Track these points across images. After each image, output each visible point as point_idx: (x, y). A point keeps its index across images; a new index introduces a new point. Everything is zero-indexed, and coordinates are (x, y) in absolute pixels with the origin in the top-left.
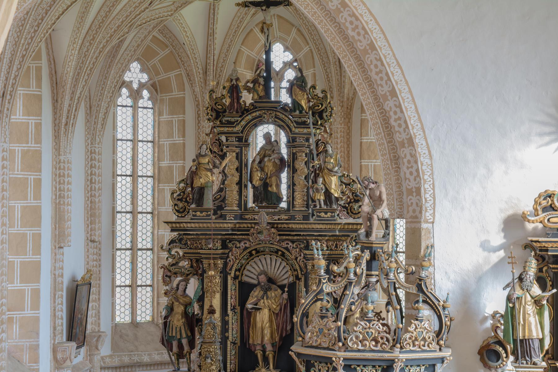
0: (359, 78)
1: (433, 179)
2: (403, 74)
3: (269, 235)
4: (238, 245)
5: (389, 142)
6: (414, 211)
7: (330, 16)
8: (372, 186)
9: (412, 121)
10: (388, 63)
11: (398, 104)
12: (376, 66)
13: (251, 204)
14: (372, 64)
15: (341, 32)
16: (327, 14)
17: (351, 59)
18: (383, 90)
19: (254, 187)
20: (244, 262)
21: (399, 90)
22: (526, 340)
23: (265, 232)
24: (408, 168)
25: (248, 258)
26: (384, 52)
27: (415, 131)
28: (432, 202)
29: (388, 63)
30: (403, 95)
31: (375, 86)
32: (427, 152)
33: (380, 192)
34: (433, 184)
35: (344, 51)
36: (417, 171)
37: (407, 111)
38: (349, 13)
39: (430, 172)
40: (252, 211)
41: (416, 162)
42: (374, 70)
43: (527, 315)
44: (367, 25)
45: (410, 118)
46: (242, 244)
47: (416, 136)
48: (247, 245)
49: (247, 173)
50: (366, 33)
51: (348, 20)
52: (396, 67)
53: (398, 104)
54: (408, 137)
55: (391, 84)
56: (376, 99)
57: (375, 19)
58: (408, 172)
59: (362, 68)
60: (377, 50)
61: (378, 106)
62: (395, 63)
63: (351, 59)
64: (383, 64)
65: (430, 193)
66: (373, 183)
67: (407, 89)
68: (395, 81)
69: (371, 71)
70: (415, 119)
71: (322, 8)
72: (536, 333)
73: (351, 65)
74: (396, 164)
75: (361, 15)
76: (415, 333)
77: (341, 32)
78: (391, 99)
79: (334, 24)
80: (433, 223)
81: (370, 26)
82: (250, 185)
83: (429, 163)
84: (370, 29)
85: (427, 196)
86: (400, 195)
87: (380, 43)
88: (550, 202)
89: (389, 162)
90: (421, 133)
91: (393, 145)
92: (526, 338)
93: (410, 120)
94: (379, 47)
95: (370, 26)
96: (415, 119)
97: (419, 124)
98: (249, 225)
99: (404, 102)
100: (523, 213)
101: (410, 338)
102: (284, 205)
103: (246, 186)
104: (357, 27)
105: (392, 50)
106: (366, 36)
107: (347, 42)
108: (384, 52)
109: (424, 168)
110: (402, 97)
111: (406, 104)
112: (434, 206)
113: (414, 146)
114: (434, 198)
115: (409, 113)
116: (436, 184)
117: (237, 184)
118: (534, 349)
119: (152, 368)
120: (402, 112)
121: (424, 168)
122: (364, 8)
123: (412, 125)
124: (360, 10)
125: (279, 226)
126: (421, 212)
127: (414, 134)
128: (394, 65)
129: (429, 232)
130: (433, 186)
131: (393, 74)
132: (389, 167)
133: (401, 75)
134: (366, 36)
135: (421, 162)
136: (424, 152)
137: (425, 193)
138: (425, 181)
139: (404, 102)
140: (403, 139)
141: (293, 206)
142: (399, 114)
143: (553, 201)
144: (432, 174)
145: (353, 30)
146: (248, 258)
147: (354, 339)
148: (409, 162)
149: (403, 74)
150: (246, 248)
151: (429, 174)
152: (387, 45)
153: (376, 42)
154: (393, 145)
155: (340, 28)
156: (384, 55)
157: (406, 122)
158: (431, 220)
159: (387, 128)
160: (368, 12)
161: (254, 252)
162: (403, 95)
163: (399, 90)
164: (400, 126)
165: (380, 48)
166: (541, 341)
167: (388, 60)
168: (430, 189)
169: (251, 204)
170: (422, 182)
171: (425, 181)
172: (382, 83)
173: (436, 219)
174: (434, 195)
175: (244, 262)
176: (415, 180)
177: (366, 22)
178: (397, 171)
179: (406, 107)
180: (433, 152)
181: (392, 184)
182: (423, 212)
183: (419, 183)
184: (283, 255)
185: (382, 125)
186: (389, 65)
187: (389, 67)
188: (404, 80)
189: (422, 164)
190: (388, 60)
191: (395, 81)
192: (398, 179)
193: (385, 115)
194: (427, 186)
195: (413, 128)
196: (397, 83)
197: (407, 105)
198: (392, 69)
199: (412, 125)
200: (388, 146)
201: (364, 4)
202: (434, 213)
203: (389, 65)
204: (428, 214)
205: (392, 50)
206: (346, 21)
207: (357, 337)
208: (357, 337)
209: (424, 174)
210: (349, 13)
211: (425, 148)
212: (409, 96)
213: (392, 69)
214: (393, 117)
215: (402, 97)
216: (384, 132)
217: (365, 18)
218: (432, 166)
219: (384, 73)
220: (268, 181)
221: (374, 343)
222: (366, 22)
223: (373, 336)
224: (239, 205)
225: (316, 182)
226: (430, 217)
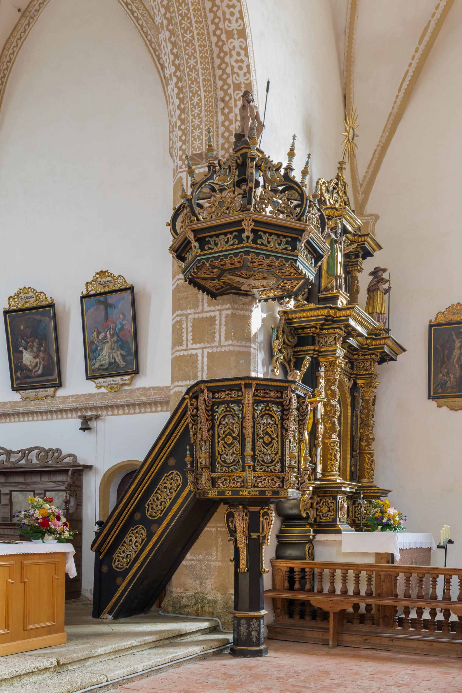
11: (244, 46)
12: (238, 54)
42: (235, 57)
53: (244, 46)
54: (246, 82)
55: (242, 23)
78: (238, 39)
100: (215, 299)
119: (54, 417)
132: (212, 104)
140: (241, 83)
142: (243, 57)
172: (231, 18)
181: (213, 122)
219: (238, 9)
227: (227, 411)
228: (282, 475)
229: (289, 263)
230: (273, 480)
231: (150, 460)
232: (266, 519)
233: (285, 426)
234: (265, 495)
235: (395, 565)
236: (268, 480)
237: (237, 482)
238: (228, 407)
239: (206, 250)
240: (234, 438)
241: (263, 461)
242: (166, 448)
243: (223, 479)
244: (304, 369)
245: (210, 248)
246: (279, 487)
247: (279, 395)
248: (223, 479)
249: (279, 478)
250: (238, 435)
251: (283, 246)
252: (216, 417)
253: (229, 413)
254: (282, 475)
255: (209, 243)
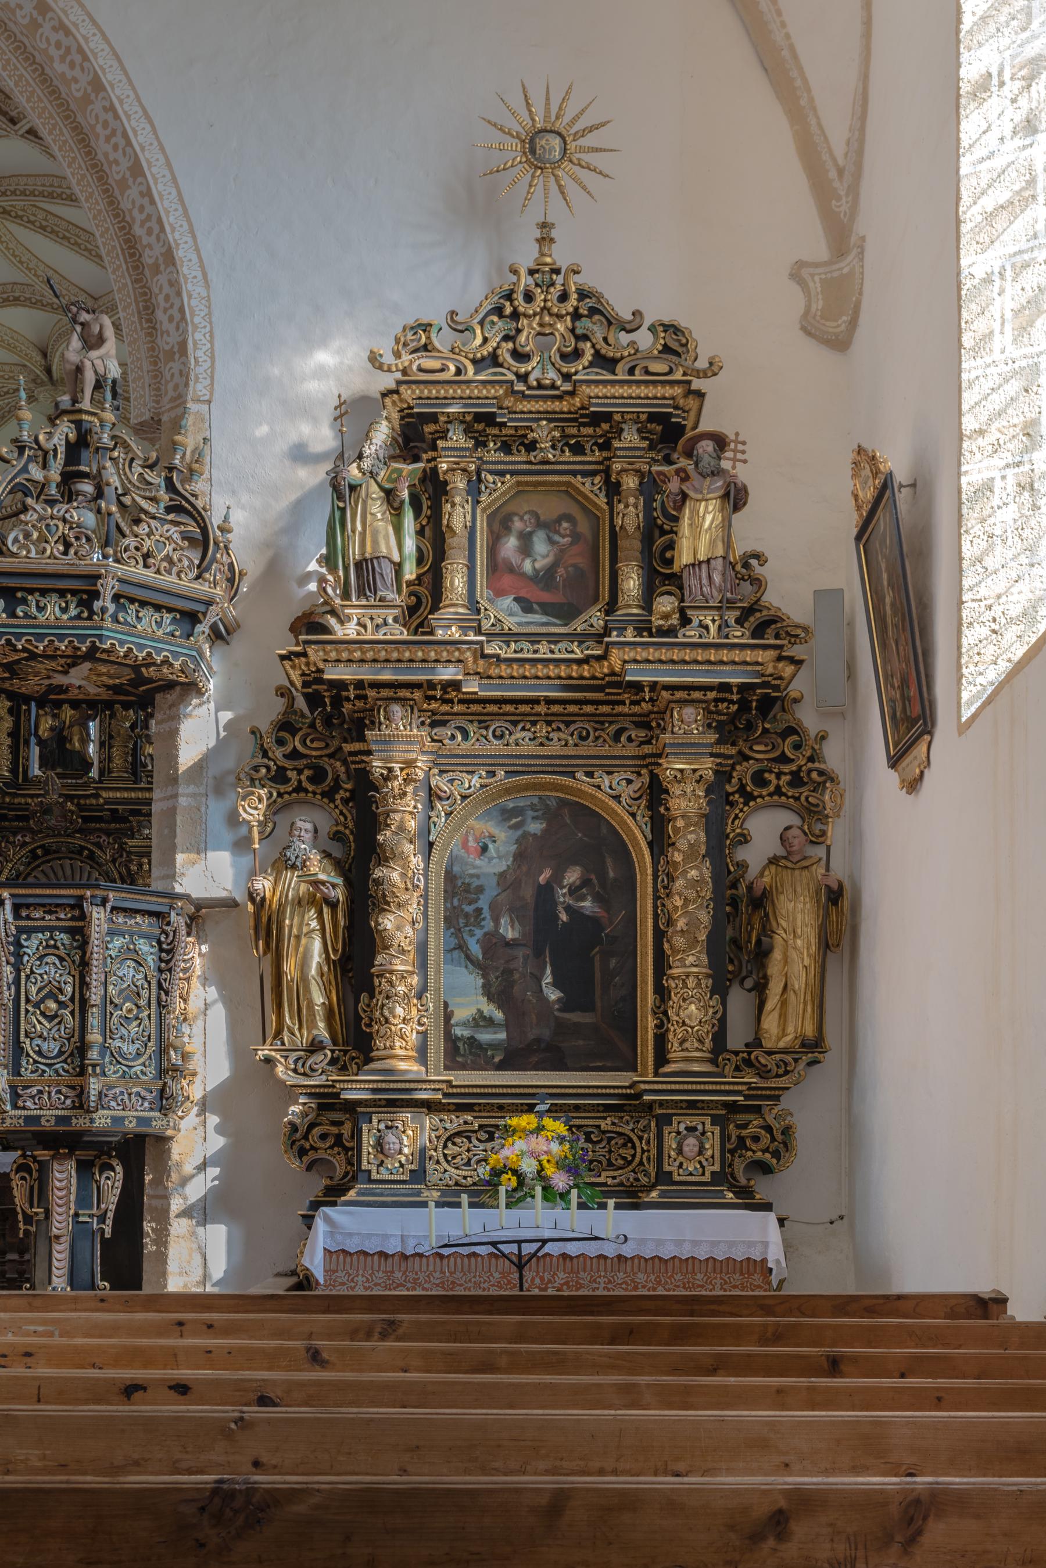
0: (80, 167)
1: (210, 323)
2: (155, 132)
3: (64, 816)
4: (11, 839)
5: (137, 281)
6: (176, 387)
7: (25, 52)
8: (84, 317)
9: (172, 219)
10: (125, 113)
13: (36, 771)
14: (98, 122)
15: (45, 80)
16: (19, 47)
17: (65, 131)
18: (495, 1282)
19: (40, 742)
20: (22, 868)
21: (148, 161)
22: (366, 560)
23: (57, 811)
24: (108, 139)
25: (29, 863)
26: (118, 92)
27: (177, 235)
28: (209, 364)
29: (125, 113)
30: (154, 170)
31: (106, 167)
32: (199, 274)
33: (101, 327)
34: (211, 332)
35: (51, 117)
36: (182, 310)
37: (162, 199)
38: (52, 23)
39: (206, 310)
40: (37, 782)
41: (179, 294)
43: (369, 516)
44: (87, 42)
45: (168, 212)
46: (19, 837)
47: (178, 245)
48: (27, 839)
49: (29, 720)
50: (86, 58)
51: (53, 41)
52: (142, 120)
56: (111, 203)
57: (103, 34)
58: (108, 148)
59: (85, 147)
60: (105, 90)
61: (116, 216)
62: (140, 113)
63: (65, 131)
64: (117, 117)
65: (204, 349)
66: (88, 312)
67: (162, 160)
68: (140, 145)
69: (97, 136)
70: (177, 214)
71: (10, 37)
72: (388, 546)
73: (65, 142)
74: (149, 321)
75: (76, 25)
76: (149, 542)
77: (45, 80)
79: (31, 65)
80: (209, 402)
81: (92, 45)
82: (33, 740)
83: (204, 294)
84: (92, 51)
85: (199, 353)
86: (156, 377)
87: (111, 76)
88: (423, 340)
89: (136, 319)
90: (190, 240)
91: (144, 286)
92: (368, 555)
93: (168, 217)
94: (109, 82)
95: (92, 45)
96: (177, 214)
97: (185, 224)
98: (30, 801)
99: (156, 184)
101: (137, 549)
102: (94, 773)
103: (27, 743)
104: (68, 50)
105: (134, 89)
106: (85, 64)
107: (56, 99)
108: (118, 92)
109: (193, 302)
110: (153, 176)
111: (160, 187)
112: (212, 373)
113: (174, 264)
114: (213, 358)
115: (166, 203)
116: (217, 333)
117: (9, 735)
118: (382, 575)
120: (153, 202)
121: (193, 302)
122: (80, 12)
123: (171, 225)
124: (74, 16)
125: (82, 802)
126: (187, 385)
127: (175, 241)
128: (137, 116)
129: (203, 420)
130: (212, 336)
131: (135, 132)
133: (151, 135)
134: (85, 64)
135: (188, 292)
136: (194, 274)
137: (195, 348)
138: (195, 328)
139: (156, 184)
141: (110, 771)
143: (428, 338)
144: (209, 314)
145: (62, 59)
146: (29, 863)
147: (21, 537)
148: (167, 298)
149: (155, 132)
150: (24, 844)
151: (202, 314)
152: (125, 80)
153: (104, 74)
154: (144, 286)
155: (43, 73)
156: (118, 98)
157: (160, 221)
158: (206, 398)
159: (132, 255)
160: (87, 20)
161: (39, 852)
162: (154, 170)
163: (148, 161)
164: (150, 232)
165: (112, 86)
166: (398, 568)
167: (126, 107)
168: (204, 341)
169: (36, 771)
170: (190, 328)
171: (195, 328)
173: (216, 395)
174: (212, 353)
175: (22, 868)
176: (178, 329)
177: (83, 36)
178: (150, 334)
179: (159, 193)
180: (212, 276)
182: (191, 383)
183: (185, 331)
184: (92, 856)
185: (122, 250)
186: (128, 117)
187: (129, 120)
188: (156, 143)
189: (190, 297)
190: (126, 107)
191: (140, 145)
192: (153, 349)
193: (129, 233)
194: (198, 336)
195: (173, 230)
196: (143, 149)
197: (161, 189)
198: (134, 123)
199: (171, 225)
200: (134, 289)
201: (82, 6)
202: (212, 384)
203: (128, 117)
204: (199, 386)
205: (134, 89)
206: (49, 43)
207: (27, 536)
208: (27, 536)
209: (193, 315)
210: (52, 23)
211: (196, 267)
212: (167, 172)
213: (134, 123)
214: (139, 217)
215: (153, 176)
216: (126, 262)
217: (82, 30)
218: (209, 300)
220: (65, 733)
221: (61, 548)
222: (83, 36)
223: (60, 533)
224: (14, 771)
225: (147, 728)
226: (204, 391)
227: (48, 946)
228: (77, 1081)
229: (66, 643)
230: (59, 1092)
231: (463, 1090)
232: (108, 1178)
233: (165, 985)
234: (39, 1124)
235: (316, 1293)
236: (49, 1093)
237: (66, 1097)
238: (52, 938)
239: (18, 617)
240: (62, 1005)
241: (39, 1053)
242: (707, 1087)
243: (34, 1091)
244: (560, 908)
245: (26, 616)
246: (74, 1108)
247: (76, 913)
248: (34, 1091)
249: (72, 1087)
250: (72, 999)
251: (73, 612)
252: (26, 958)
253: (52, 951)
254: (77, 1081)
255: (24, 601)
